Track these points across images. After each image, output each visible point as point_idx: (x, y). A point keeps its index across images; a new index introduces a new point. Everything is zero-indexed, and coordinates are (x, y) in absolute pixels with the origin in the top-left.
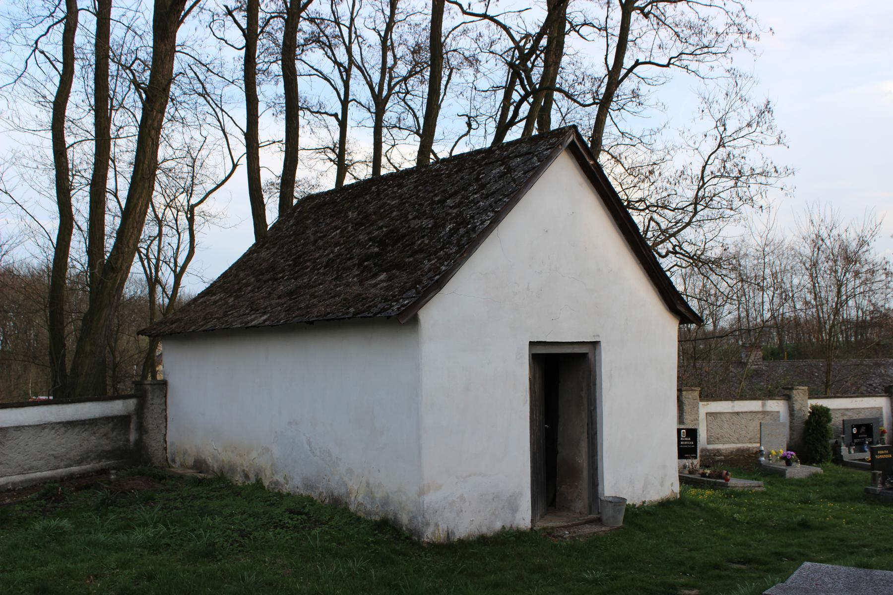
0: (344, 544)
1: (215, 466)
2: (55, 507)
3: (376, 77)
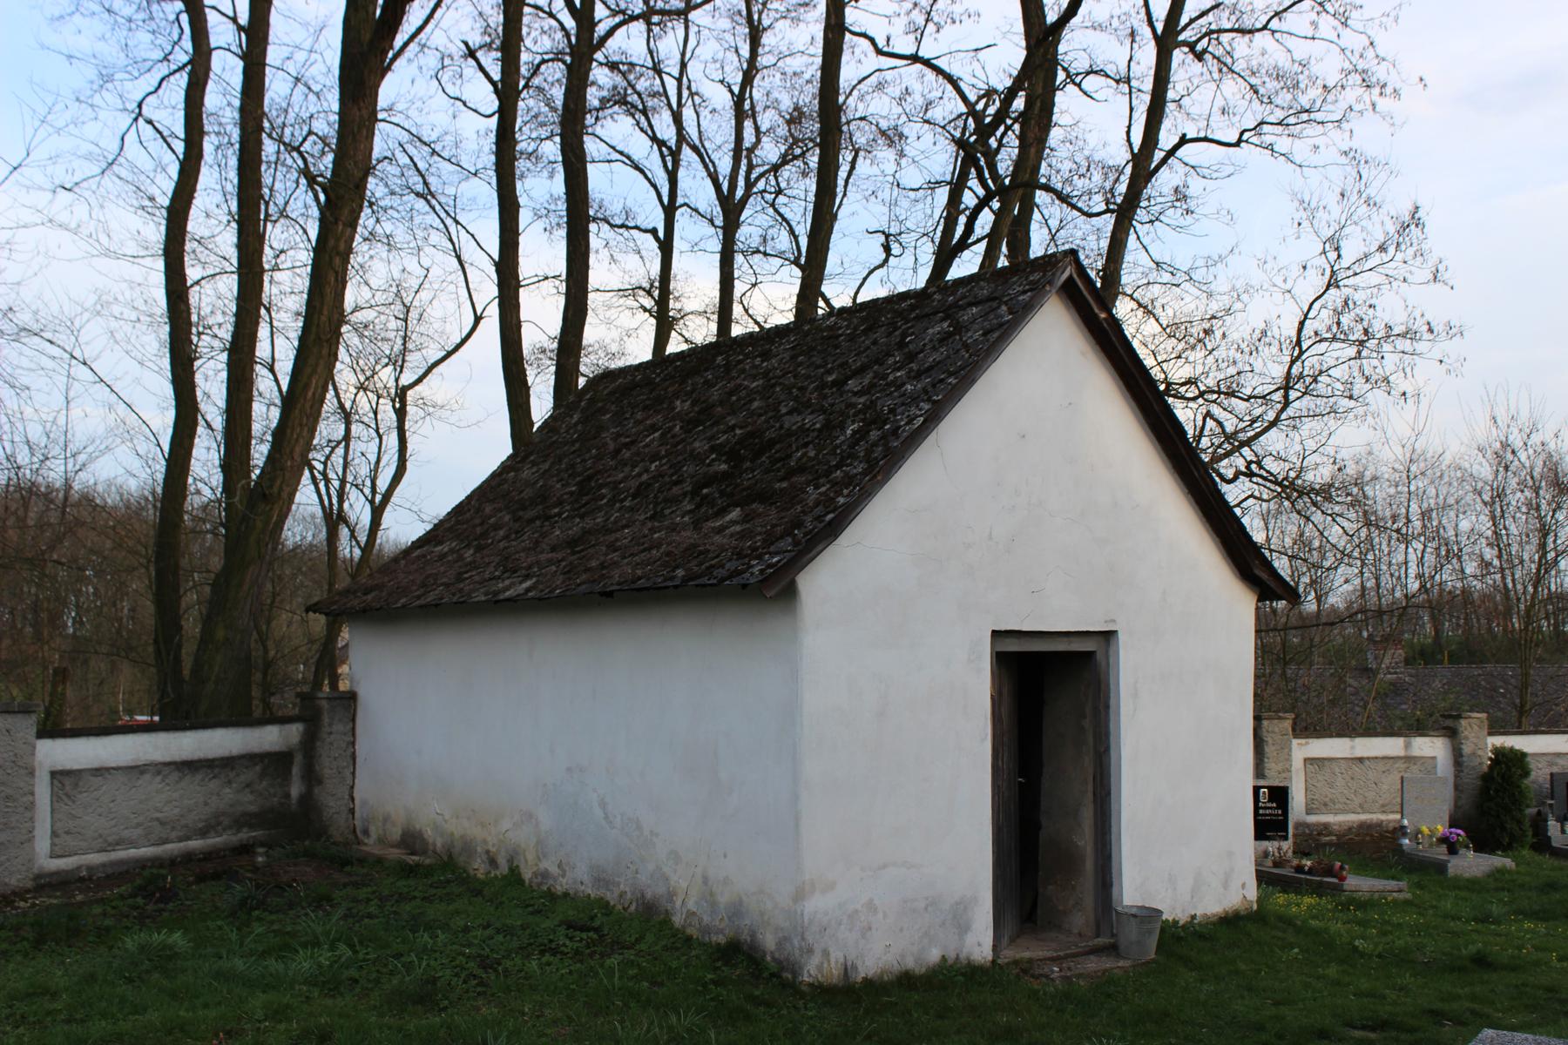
0: (661, 984)
1: (439, 845)
3: (724, 166)
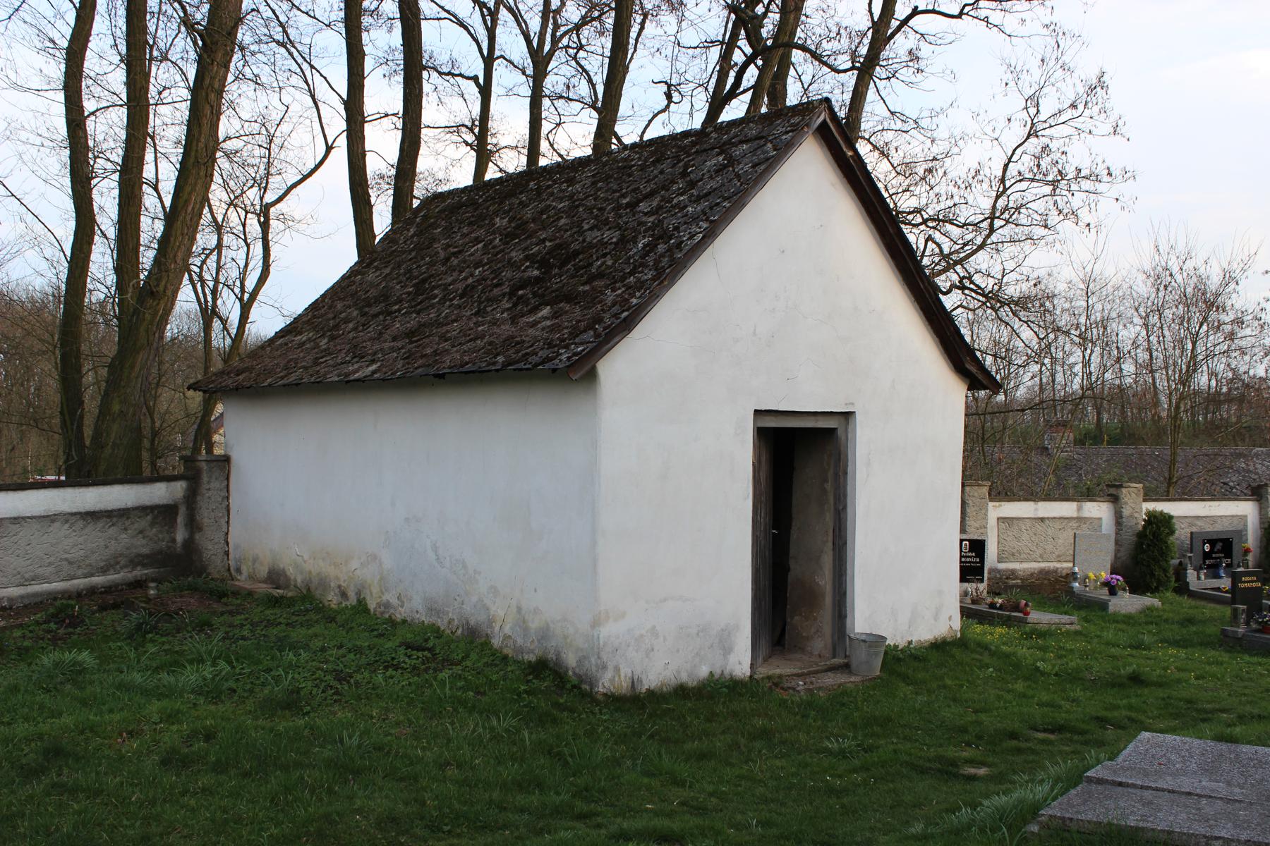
0: (484, 694)
1: (299, 580)
2: (70, 634)
3: (535, 24)
